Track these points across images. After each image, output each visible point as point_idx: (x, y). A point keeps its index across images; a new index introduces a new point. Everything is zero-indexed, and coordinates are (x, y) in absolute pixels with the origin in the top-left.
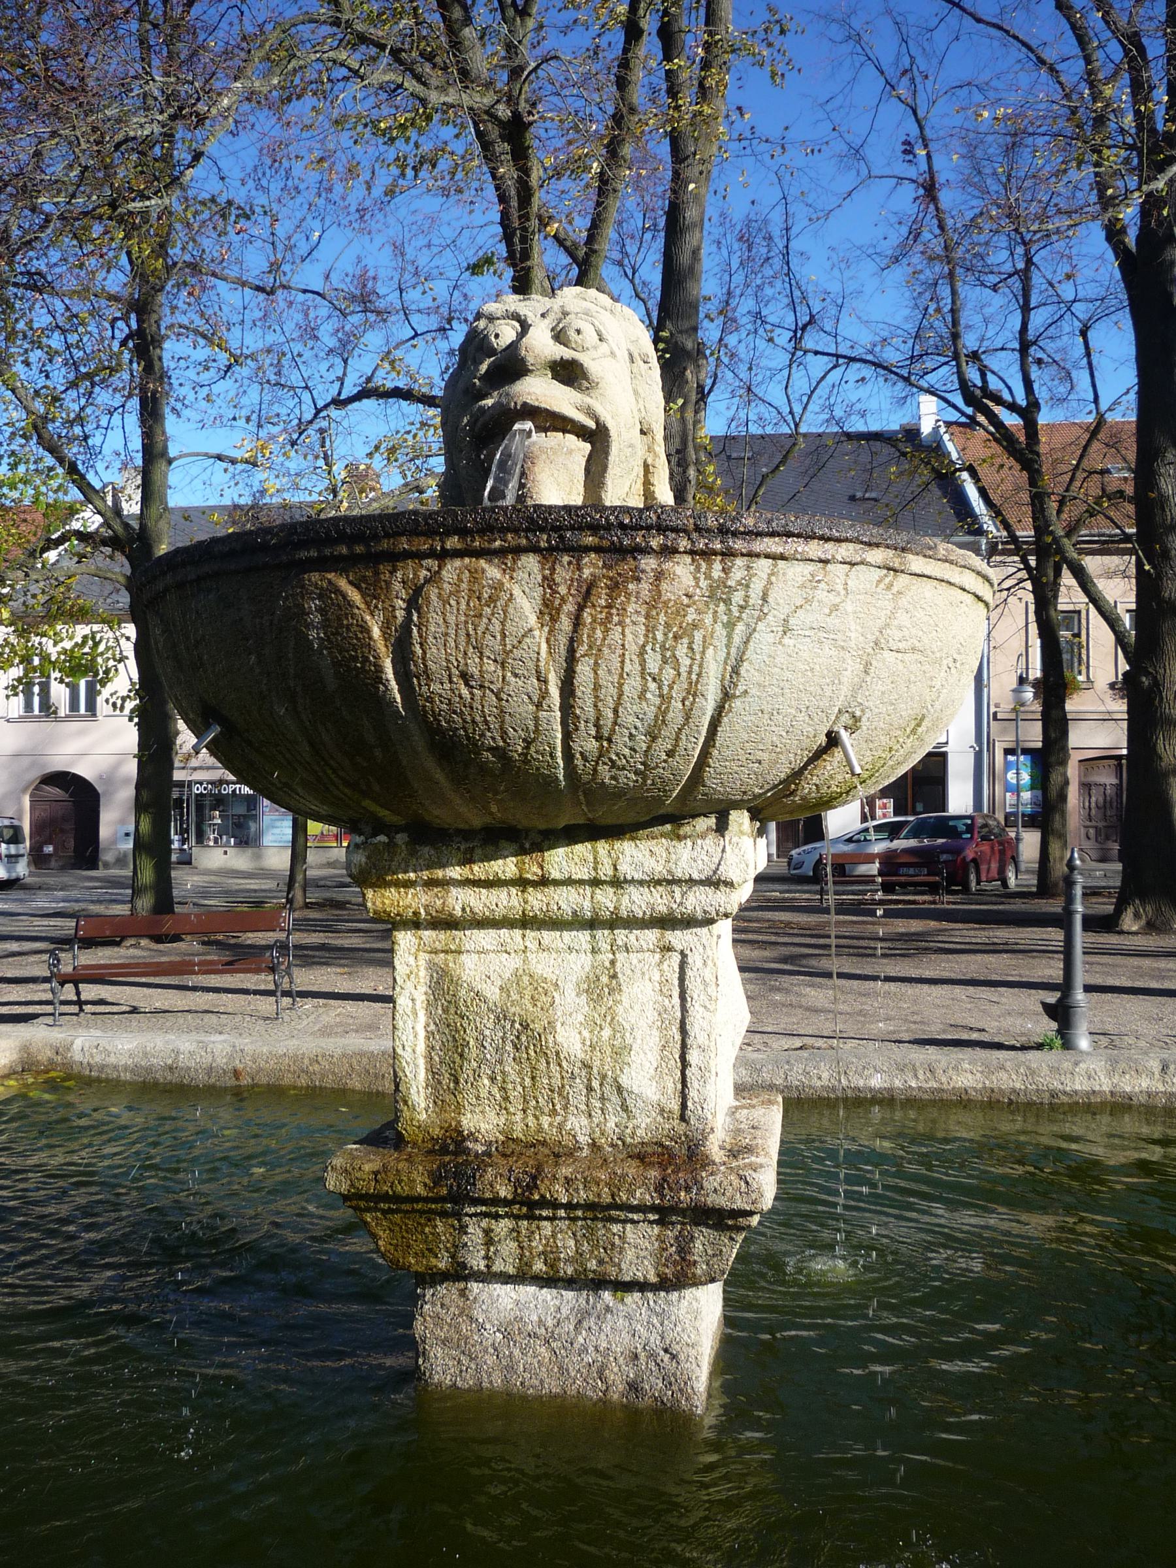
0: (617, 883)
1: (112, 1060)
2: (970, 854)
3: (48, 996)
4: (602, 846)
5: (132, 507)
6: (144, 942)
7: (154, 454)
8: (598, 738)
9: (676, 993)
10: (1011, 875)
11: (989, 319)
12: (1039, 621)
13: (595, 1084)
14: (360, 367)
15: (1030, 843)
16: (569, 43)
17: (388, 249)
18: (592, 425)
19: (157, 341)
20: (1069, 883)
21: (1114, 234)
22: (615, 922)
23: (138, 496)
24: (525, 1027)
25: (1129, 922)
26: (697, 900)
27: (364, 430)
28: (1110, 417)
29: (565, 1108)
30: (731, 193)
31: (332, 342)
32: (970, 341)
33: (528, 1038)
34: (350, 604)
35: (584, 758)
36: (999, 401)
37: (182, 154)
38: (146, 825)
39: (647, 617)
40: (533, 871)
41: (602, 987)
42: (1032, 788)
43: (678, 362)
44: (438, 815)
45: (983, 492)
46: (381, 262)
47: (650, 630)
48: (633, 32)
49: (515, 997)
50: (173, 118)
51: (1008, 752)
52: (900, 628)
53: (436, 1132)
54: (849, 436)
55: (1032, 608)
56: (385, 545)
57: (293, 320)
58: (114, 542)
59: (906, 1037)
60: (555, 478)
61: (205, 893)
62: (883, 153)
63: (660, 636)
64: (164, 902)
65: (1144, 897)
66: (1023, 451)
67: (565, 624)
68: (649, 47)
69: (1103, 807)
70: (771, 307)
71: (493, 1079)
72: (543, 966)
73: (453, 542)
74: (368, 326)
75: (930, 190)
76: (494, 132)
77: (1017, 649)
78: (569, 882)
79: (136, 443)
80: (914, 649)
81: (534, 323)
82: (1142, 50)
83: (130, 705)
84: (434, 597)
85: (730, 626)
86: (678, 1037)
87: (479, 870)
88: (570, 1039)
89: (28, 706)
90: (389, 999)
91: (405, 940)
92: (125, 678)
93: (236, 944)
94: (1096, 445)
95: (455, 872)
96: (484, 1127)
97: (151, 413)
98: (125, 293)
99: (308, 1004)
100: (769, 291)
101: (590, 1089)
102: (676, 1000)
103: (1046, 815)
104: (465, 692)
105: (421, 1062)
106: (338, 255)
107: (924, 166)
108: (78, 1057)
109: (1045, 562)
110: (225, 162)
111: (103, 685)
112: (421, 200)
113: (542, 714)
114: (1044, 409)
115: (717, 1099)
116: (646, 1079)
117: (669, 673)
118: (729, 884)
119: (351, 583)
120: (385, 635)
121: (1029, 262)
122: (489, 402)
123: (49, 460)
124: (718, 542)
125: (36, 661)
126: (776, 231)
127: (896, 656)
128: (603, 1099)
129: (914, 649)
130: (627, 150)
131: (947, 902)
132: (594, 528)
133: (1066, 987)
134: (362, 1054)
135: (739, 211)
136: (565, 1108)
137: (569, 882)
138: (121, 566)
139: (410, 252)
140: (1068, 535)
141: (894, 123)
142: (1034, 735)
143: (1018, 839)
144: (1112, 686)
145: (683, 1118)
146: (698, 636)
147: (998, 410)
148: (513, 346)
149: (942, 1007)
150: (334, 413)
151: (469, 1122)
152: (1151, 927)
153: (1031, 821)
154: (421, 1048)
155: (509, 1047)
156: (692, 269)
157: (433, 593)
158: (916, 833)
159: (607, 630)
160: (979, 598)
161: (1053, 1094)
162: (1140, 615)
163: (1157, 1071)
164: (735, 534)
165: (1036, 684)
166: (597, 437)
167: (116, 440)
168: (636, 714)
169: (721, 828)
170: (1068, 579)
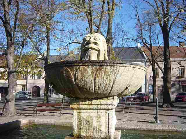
0: (100, 105)
1: (40, 122)
2: (144, 97)
3: (33, 113)
4: (99, 100)
5: (46, 55)
6: (45, 106)
7: (48, 49)
8: (98, 88)
9: (108, 118)
10: (149, 100)
11: (146, 34)
12: (152, 69)
13: (98, 129)
14: (73, 39)
15: (152, 96)
16: (97, 3)
17: (76, 27)
18: (98, 50)
19: (49, 37)
20: (157, 102)
21: (160, 25)
22: (100, 110)
23: (46, 54)
24: (89, 122)
25: (164, 106)
26: (109, 107)
27: (72, 47)
28: (160, 46)
29: (94, 132)
30: (115, 21)
31: (69, 37)
32: (144, 37)
33: (89, 124)
34: (69, 71)
35: (97, 90)
36: (147, 44)
37: (52, 16)
38: (46, 93)
39: (104, 73)
40: (90, 103)
41: (98, 117)
42: (152, 89)
43: (109, 40)
44: (79, 96)
45: (145, 54)
46: (75, 28)
47: (105, 75)
48: (104, 3)
49: (88, 118)
50: (52, 12)
51: (149, 85)
52: (135, 75)
53: (78, 135)
54: (129, 47)
55: (152, 68)
56: (73, 64)
57: (64, 34)
58: (43, 59)
59: (136, 120)
60: (94, 57)
61: (52, 100)
62: (133, 16)
63: (106, 76)
64: (48, 102)
65: (166, 103)
66: (150, 50)
67: (94, 74)
68: (106, 4)
69: (161, 92)
70: (120, 33)
71: (85, 128)
72: (92, 115)
73: (81, 64)
74: (73, 35)
75: (139, 19)
76: (88, 14)
77: (150, 72)
78: (95, 104)
79: (46, 48)
80: (137, 77)
81: (92, 37)
82: (163, 4)
83: (44, 78)
84: (79, 71)
85: (114, 74)
86: (108, 124)
87: (84, 103)
88: (94, 124)
89: (33, 78)
90: (73, 114)
91: (75, 111)
92: (44, 75)
93: (56, 107)
94: (159, 49)
95: (81, 103)
96: (84, 134)
97: (48, 45)
98: (45, 31)
99: (64, 115)
100: (120, 31)
101: (97, 130)
102: (108, 119)
103: (154, 93)
104: (82, 82)
105: (76, 126)
106: (70, 27)
107: (138, 17)
108: (36, 122)
109: (153, 63)
110: (57, 17)
111: (42, 76)
112: (79, 21)
113: (92, 85)
114: (152, 45)
115: (113, 131)
116: (104, 129)
117: (107, 80)
118: (114, 105)
119: (69, 69)
120: (73, 75)
121: (150, 28)
122: (86, 47)
123: (36, 50)
124: (113, 64)
125: (34, 73)
126: (121, 24)
127: (134, 77)
128: (98, 131)
129: (137, 77)
130: (103, 16)
131: (141, 103)
132: (98, 63)
133: (156, 114)
134: (70, 122)
135: (116, 22)
136: (94, 132)
137: (95, 104)
138: (44, 62)
139: (78, 27)
140: (156, 60)
141: (135, 12)
142: (152, 83)
143: (150, 96)
144: (161, 77)
145: (108, 134)
146: (110, 75)
147: (147, 45)
148: (89, 40)
149: (141, 117)
150: (69, 45)
151: (82, 134)
152: (167, 107)
153: (152, 94)
154: (76, 124)
155: (87, 125)
156: (111, 28)
157: (79, 70)
158: (138, 95)
159: (99, 75)
160: (145, 71)
161: (155, 129)
162: (165, 69)
163: (168, 127)
164: (115, 63)
165: (152, 77)
166: (99, 51)
167: (44, 49)
168: (103, 85)
169: (113, 98)
170: (156, 65)
